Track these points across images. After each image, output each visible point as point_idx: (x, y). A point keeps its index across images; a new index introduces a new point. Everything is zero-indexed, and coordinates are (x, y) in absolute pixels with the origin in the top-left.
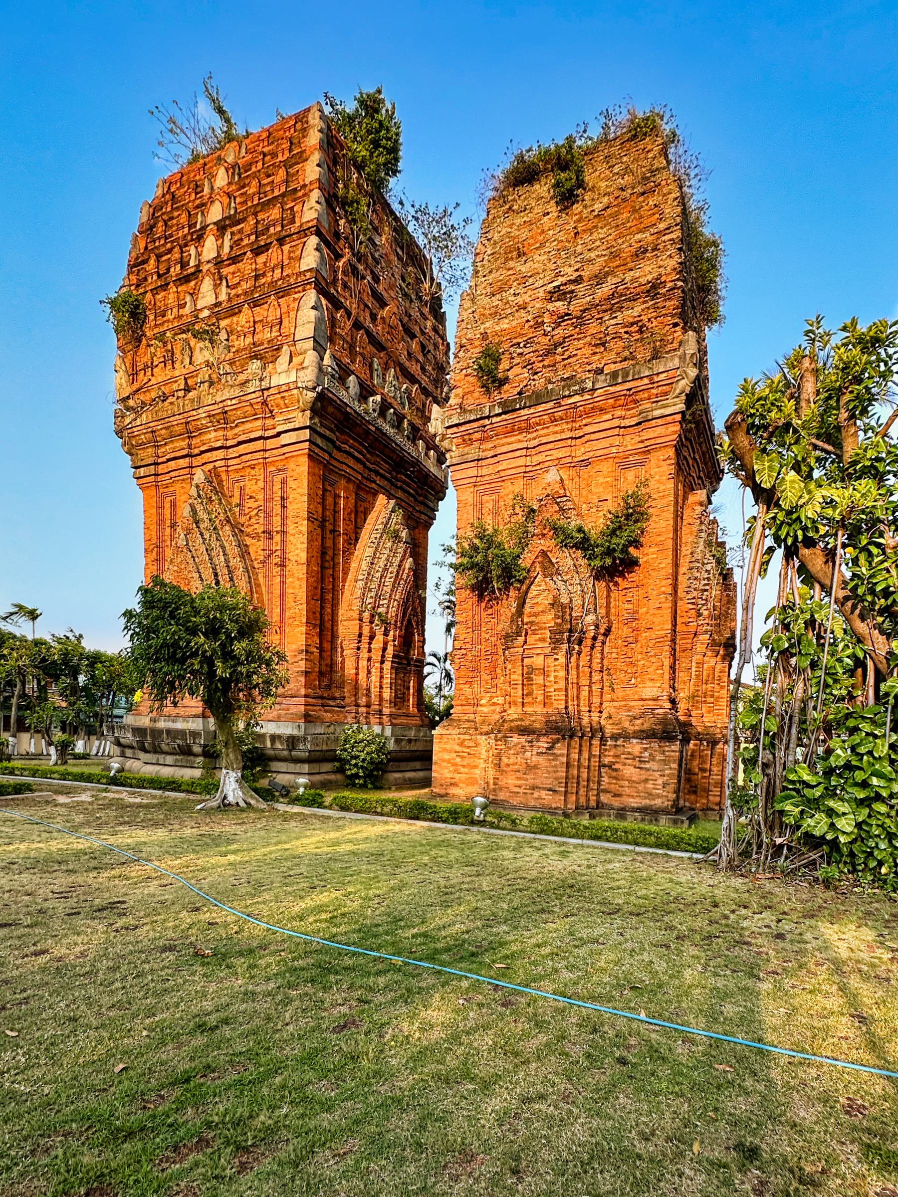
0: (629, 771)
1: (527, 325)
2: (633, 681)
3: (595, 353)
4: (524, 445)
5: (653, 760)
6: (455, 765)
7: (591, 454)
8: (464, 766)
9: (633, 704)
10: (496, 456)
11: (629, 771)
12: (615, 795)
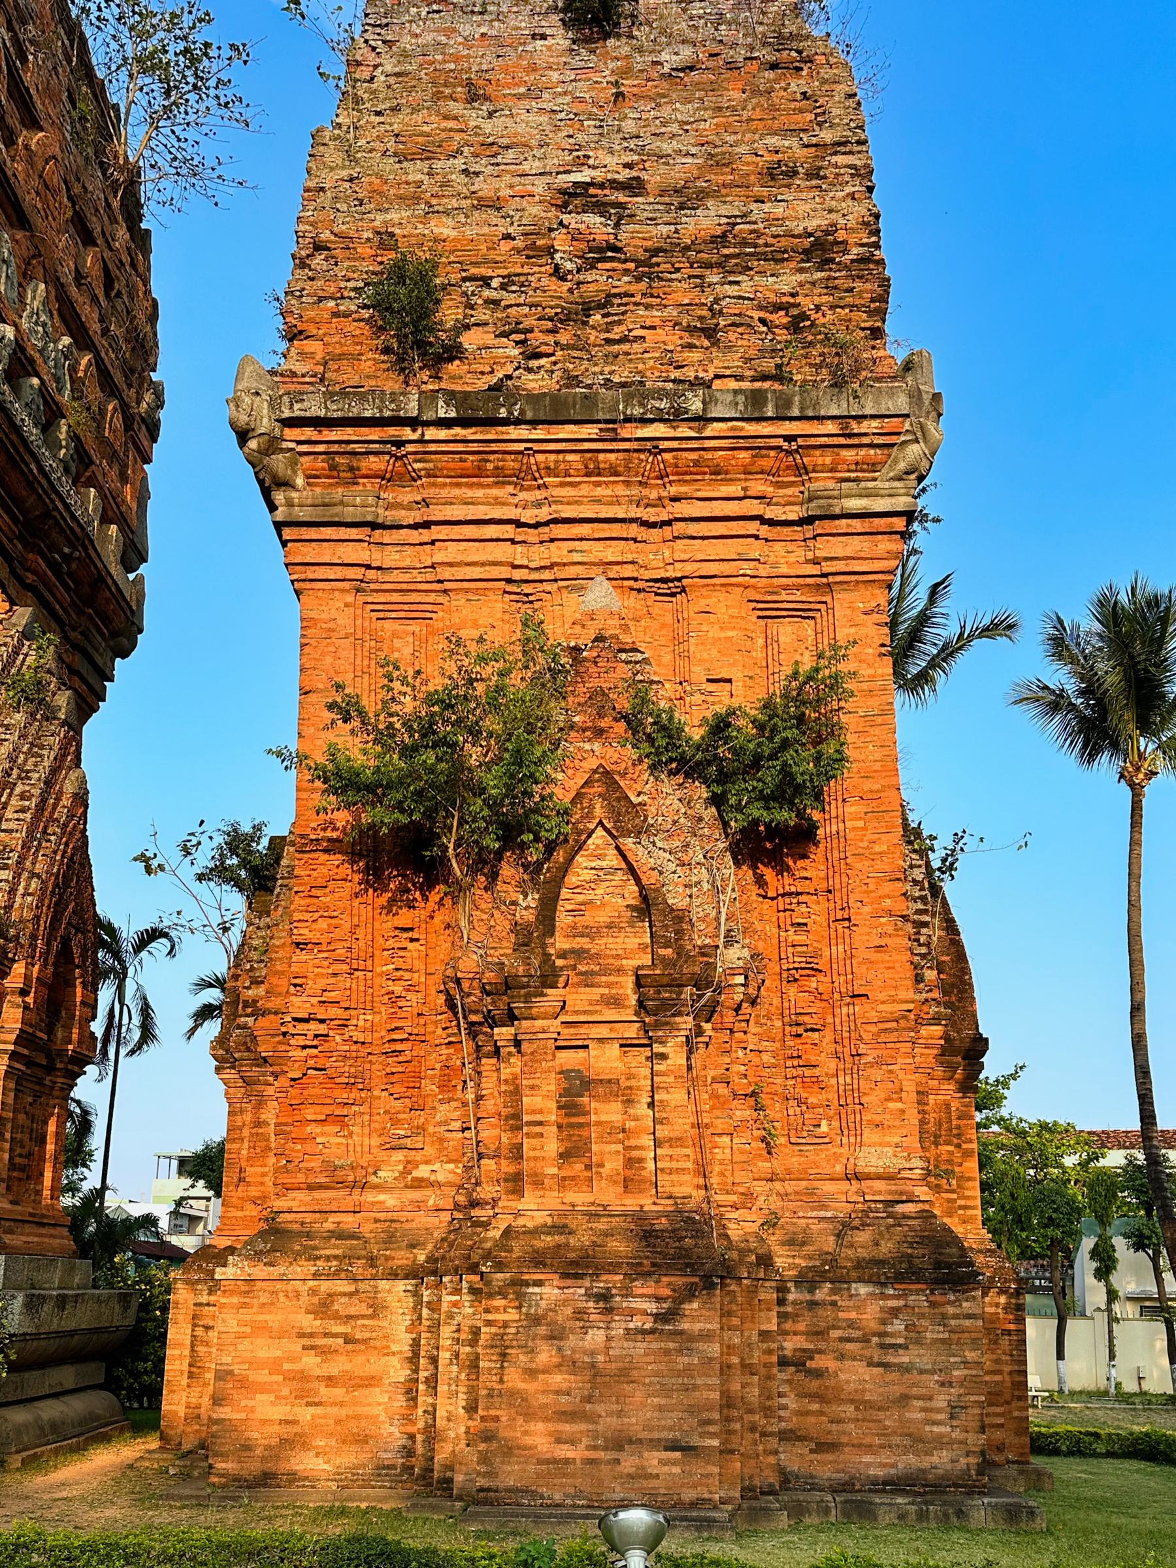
0: (855, 1375)
1: (505, 246)
2: (824, 1127)
3: (691, 346)
4: (512, 513)
5: (918, 1342)
6: (302, 1376)
7: (689, 568)
8: (330, 1381)
9: (829, 1187)
10: (427, 525)
11: (855, 1375)
12: (823, 1447)
